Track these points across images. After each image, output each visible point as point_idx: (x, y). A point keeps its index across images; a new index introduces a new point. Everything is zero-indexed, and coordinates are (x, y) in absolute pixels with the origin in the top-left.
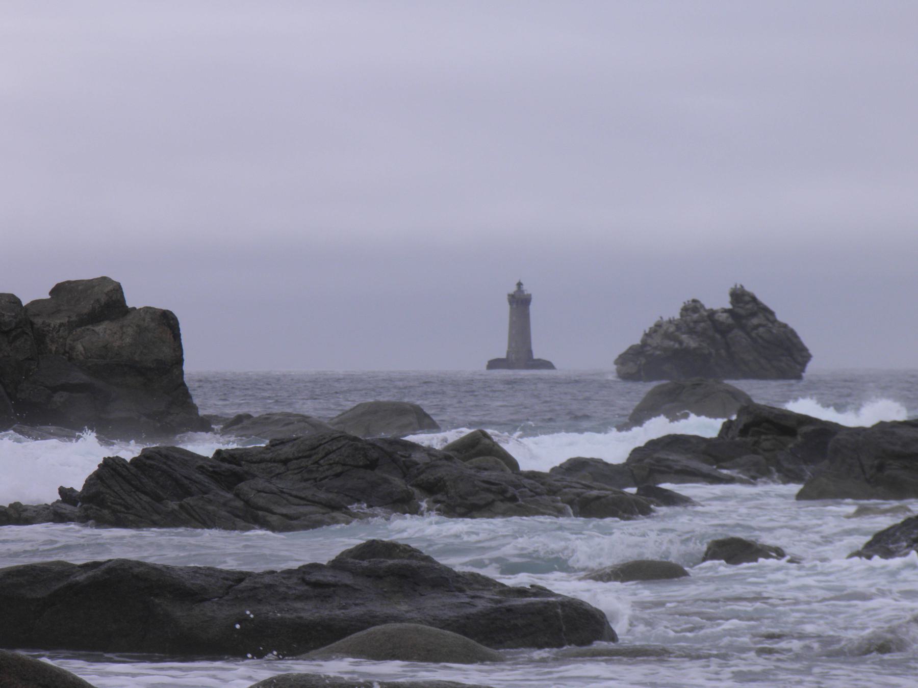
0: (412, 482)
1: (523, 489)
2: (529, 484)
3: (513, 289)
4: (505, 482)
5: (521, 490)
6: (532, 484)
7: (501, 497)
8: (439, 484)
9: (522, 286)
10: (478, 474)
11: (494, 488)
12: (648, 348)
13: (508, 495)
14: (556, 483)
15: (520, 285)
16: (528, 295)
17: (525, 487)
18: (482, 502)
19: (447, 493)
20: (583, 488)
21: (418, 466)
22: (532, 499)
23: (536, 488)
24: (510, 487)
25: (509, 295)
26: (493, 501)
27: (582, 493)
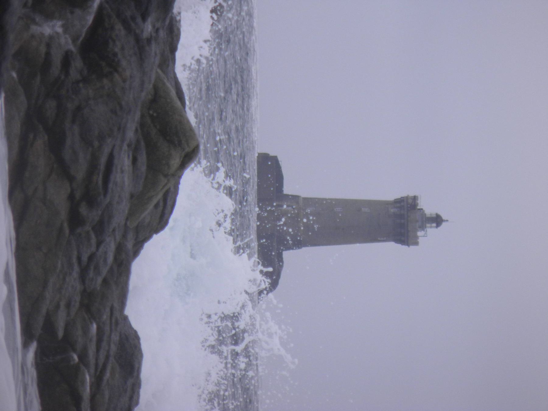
0: (107, 6)
1: (94, 241)
2: (106, 253)
4: (110, 204)
5: (93, 236)
6: (105, 260)
7: (78, 195)
8: (103, 64)
9: (434, 225)
10: (125, 147)
11: (99, 179)
13: (83, 210)
14: (108, 310)
15: (437, 220)
16: (417, 237)
17: (99, 244)
18: (67, 155)
19: (85, 80)
20: (97, 365)
21: (139, 20)
22: (75, 260)
23: (97, 268)
24: (100, 212)
25: (415, 198)
26: (71, 179)
27: (87, 366)
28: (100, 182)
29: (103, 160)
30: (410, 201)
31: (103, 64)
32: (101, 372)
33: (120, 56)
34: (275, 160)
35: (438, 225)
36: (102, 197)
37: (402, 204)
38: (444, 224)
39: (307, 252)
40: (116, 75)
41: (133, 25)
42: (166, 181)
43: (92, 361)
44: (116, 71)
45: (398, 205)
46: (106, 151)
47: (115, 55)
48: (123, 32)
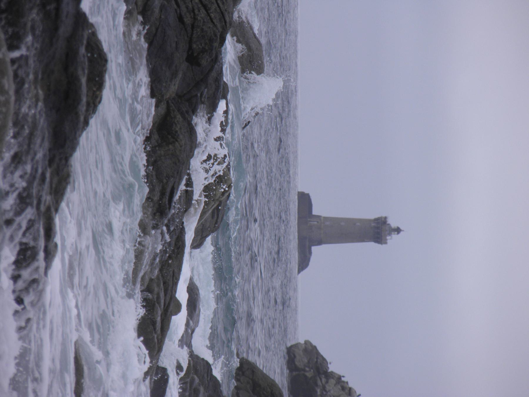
3: (393, 223)
8: (170, 137)
9: (396, 233)
11: (166, 200)
12: (324, 380)
15: (398, 230)
16: (386, 240)
19: (160, 146)
21: (191, 113)
25: (386, 218)
27: (159, 303)
28: (167, 202)
29: (168, 190)
30: (383, 219)
31: (170, 137)
32: (167, 306)
33: (179, 132)
34: (308, 195)
35: (399, 232)
36: (168, 210)
37: (379, 221)
38: (402, 233)
39: (324, 247)
40: (177, 143)
41: (187, 116)
42: (213, 204)
43: (162, 301)
44: (177, 141)
45: (376, 222)
46: (170, 185)
47: (176, 132)
48: (181, 119)
